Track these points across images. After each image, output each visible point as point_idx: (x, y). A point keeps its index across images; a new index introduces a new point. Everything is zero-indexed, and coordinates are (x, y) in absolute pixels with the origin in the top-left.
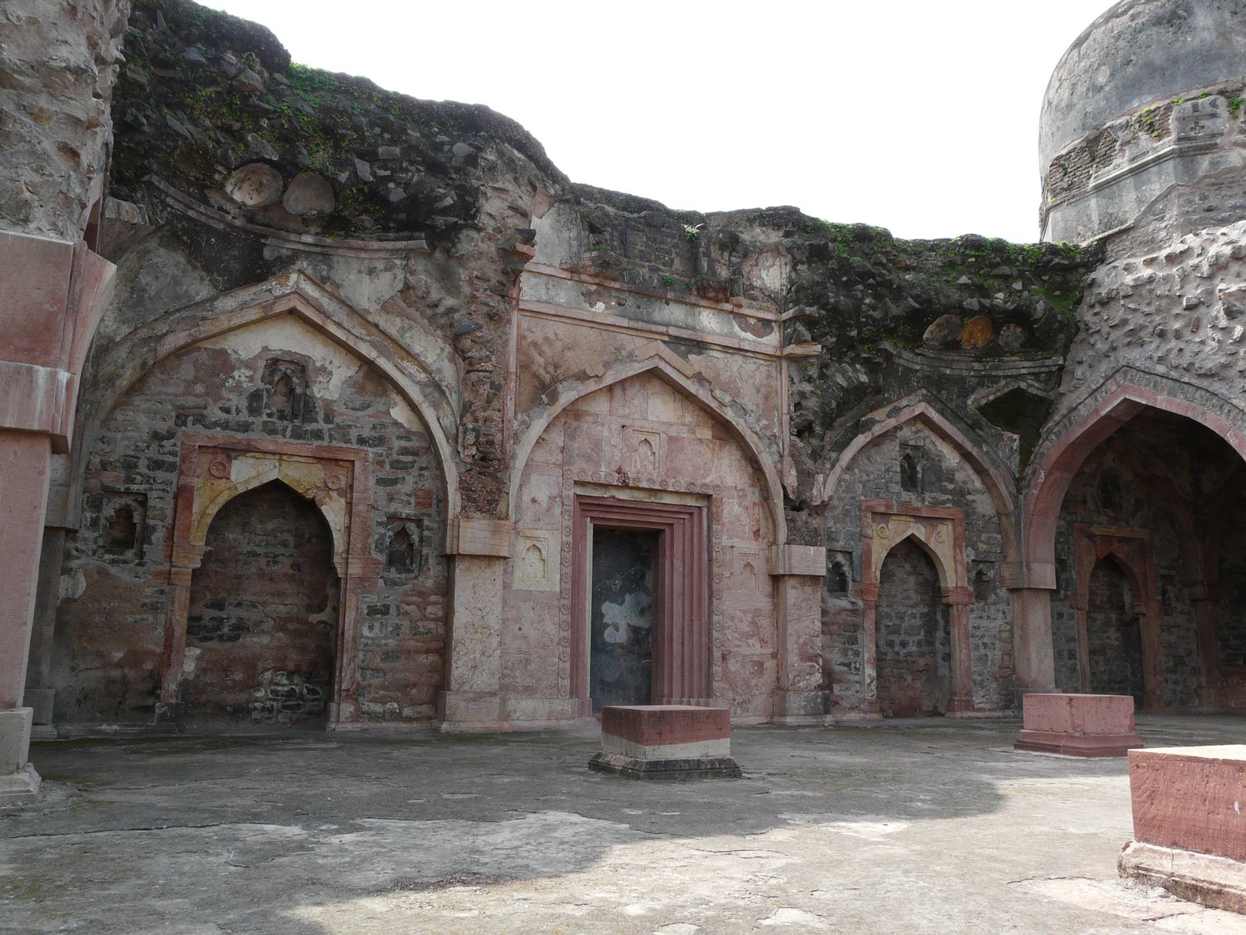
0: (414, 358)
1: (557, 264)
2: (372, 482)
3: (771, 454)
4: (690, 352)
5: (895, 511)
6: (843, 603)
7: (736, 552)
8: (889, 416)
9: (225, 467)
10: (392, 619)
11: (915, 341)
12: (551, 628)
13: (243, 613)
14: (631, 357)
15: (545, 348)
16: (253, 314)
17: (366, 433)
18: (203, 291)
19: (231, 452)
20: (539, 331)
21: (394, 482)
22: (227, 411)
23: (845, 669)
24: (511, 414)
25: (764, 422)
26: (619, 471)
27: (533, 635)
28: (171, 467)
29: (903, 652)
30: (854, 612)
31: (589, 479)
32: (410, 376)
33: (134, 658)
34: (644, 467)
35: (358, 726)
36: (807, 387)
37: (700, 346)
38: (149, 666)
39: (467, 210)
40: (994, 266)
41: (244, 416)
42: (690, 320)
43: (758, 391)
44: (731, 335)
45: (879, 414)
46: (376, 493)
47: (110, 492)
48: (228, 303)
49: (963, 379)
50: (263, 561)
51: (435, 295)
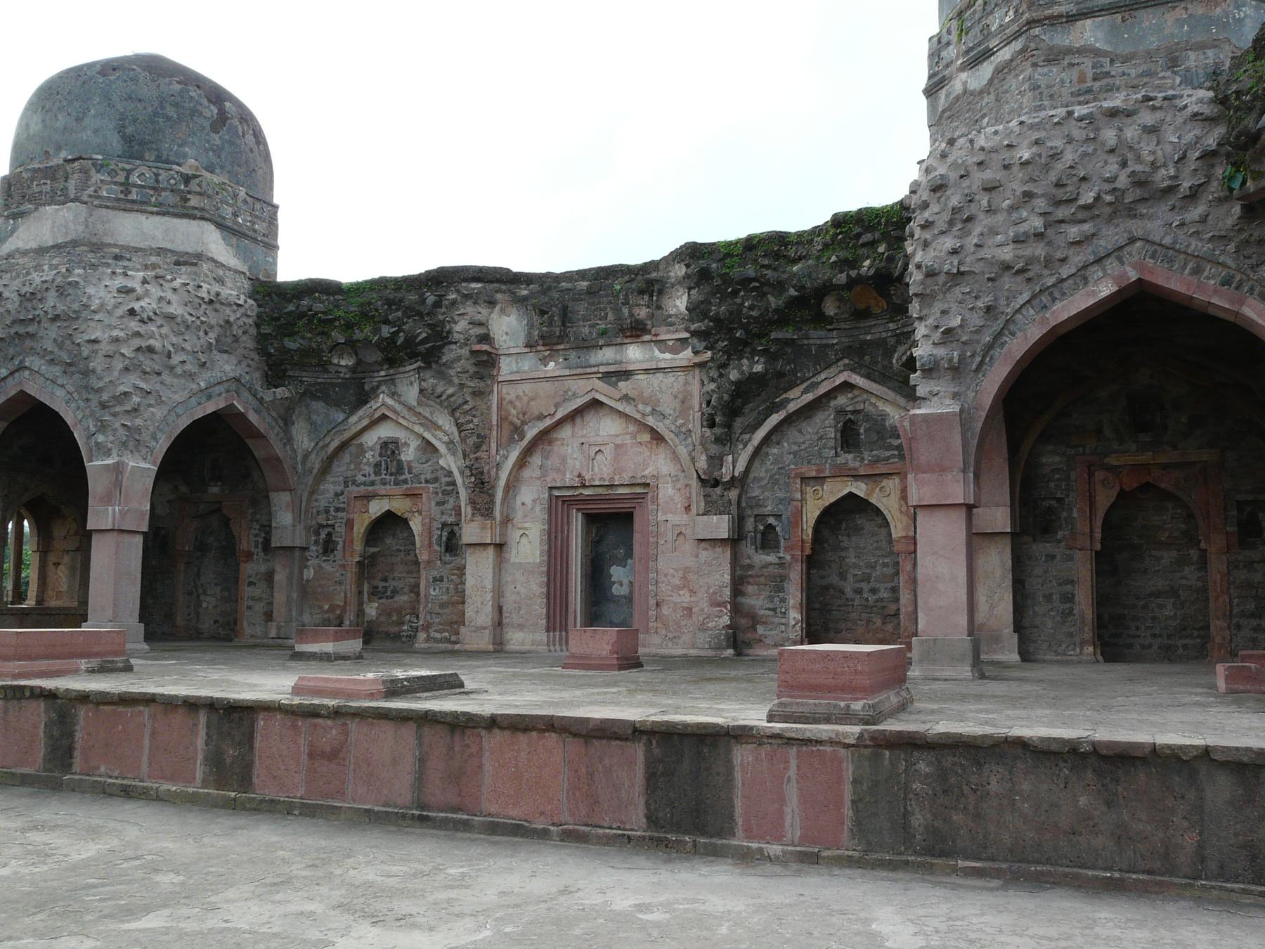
0: (439, 428)
1: (521, 344)
2: (433, 504)
3: (686, 446)
4: (620, 380)
5: (827, 474)
6: (771, 558)
7: (669, 525)
8: (805, 392)
9: (367, 506)
10: (445, 585)
11: (820, 319)
12: (535, 587)
13: (395, 583)
14: (575, 395)
15: (518, 403)
16: (365, 422)
17: (429, 476)
18: (341, 417)
19: (368, 497)
20: (510, 393)
21: (443, 503)
22: (364, 476)
23: (771, 613)
24: (494, 452)
25: (680, 421)
26: (580, 476)
27: (523, 591)
28: (343, 510)
29: (872, 598)
30: (781, 565)
31: (558, 485)
32: (440, 439)
33: (332, 609)
34: (601, 471)
35: (427, 645)
36: (713, 386)
37: (627, 374)
38: (338, 612)
39: (441, 337)
40: (858, 236)
41: (373, 477)
42: (618, 357)
43: (676, 397)
44: (651, 359)
45: (792, 394)
46: (435, 510)
47: (321, 526)
48: (353, 419)
49: (884, 340)
50: (402, 554)
51: (439, 390)
